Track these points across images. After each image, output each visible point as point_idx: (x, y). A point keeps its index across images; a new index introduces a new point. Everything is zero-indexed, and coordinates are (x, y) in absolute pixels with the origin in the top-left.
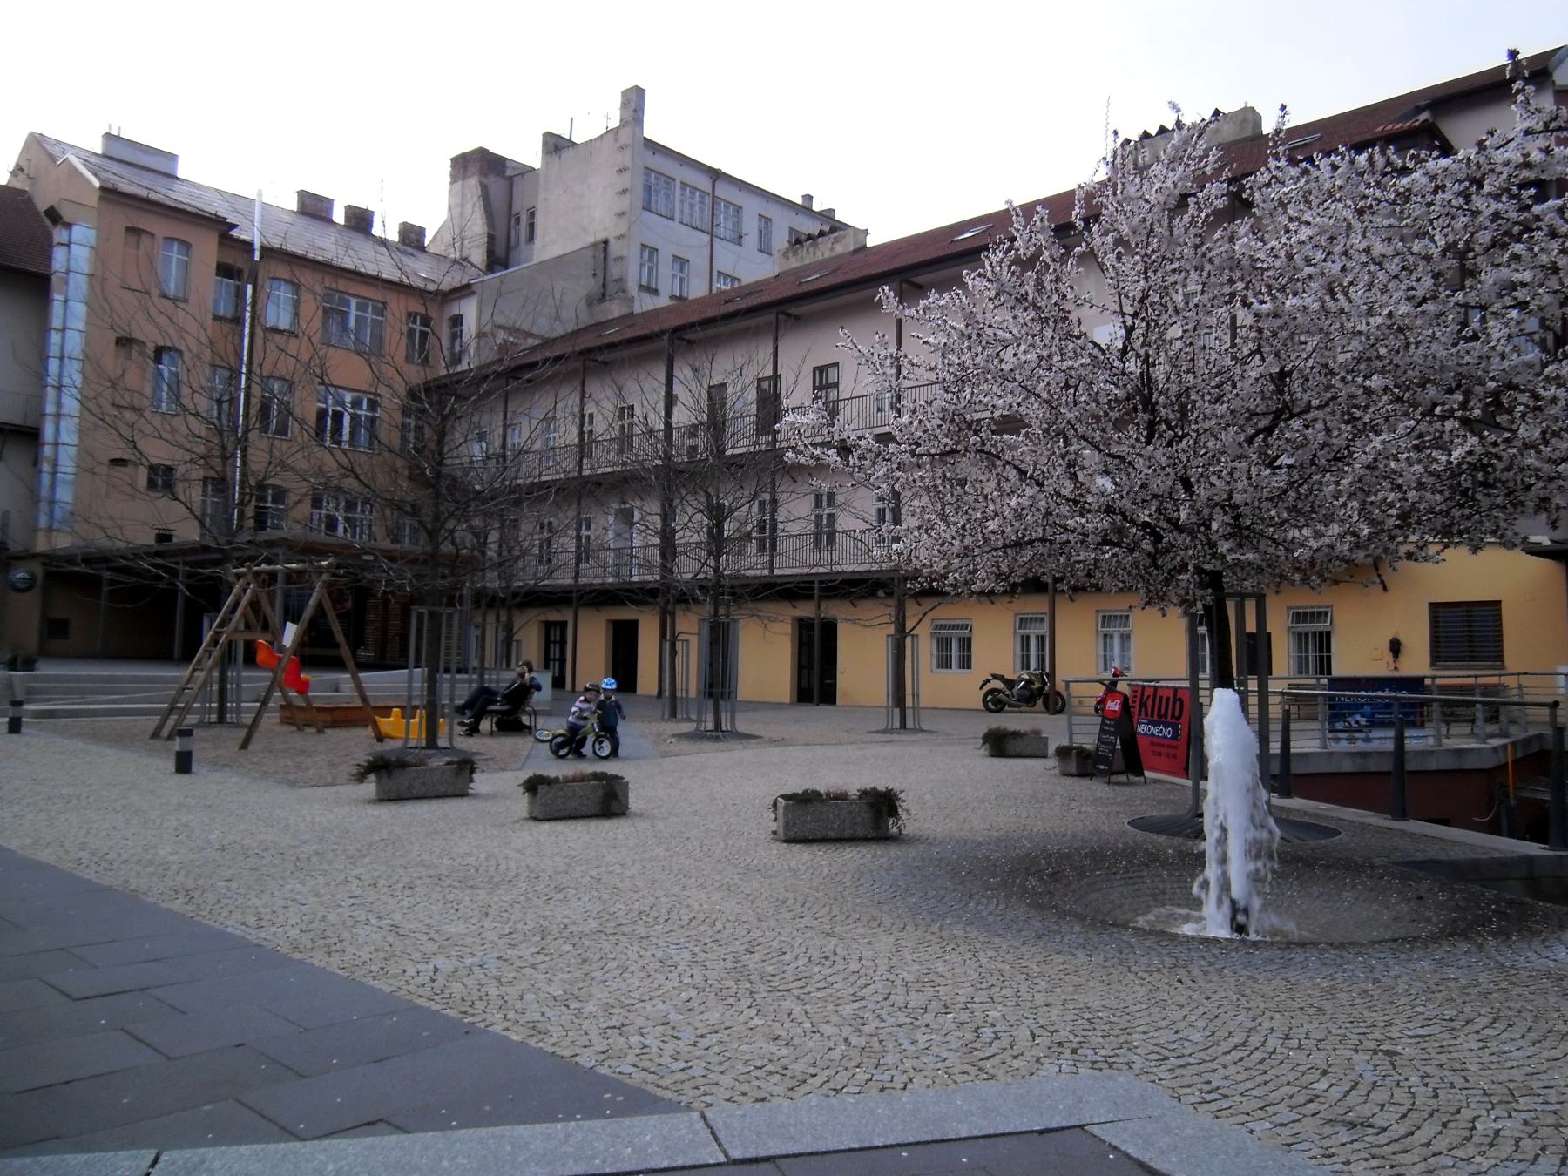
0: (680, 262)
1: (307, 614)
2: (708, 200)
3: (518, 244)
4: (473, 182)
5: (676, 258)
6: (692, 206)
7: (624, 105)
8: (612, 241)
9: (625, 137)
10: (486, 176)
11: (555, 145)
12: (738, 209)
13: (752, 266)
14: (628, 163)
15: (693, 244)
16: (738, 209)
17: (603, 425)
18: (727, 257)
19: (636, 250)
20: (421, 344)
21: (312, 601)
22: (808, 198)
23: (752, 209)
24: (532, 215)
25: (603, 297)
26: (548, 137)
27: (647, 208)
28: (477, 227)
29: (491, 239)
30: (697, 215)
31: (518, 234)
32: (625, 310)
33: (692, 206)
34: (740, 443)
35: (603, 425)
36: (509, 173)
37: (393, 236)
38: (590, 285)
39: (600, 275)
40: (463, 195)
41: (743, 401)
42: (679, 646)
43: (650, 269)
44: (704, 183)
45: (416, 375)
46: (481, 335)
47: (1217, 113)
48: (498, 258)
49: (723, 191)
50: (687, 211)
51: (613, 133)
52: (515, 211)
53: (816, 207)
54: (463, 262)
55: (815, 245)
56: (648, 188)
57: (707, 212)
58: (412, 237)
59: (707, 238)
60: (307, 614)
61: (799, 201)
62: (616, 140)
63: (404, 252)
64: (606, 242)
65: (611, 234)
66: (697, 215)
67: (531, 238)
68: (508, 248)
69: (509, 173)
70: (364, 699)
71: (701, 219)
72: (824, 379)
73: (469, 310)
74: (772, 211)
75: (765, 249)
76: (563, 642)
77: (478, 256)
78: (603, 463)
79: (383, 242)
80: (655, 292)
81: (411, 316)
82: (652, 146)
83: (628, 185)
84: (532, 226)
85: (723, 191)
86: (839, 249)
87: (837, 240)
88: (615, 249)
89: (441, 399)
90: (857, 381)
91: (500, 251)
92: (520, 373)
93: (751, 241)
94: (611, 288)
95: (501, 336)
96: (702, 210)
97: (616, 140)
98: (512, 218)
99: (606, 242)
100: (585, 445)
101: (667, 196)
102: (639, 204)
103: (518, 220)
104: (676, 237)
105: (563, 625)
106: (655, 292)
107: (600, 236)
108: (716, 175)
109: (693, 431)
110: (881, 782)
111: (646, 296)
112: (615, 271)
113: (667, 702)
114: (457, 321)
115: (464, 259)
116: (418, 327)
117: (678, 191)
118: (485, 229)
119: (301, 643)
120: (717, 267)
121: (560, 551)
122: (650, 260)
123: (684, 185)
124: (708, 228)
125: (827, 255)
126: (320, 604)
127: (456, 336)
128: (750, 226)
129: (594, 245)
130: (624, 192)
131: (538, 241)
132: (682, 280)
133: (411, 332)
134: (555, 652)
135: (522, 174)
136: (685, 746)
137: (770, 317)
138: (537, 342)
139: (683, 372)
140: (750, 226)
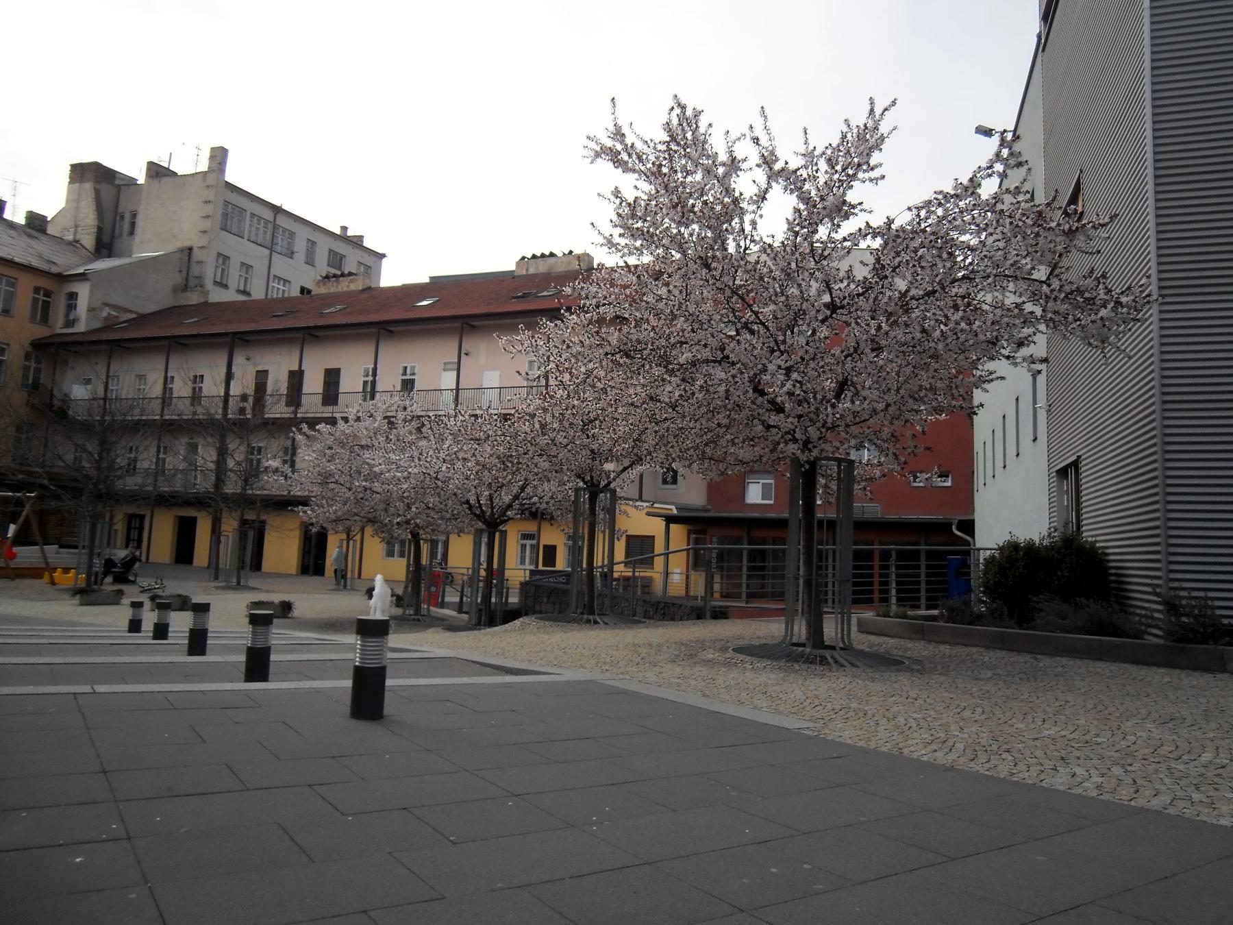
0: (247, 267)
1: (22, 519)
2: (270, 226)
3: (121, 235)
4: (88, 187)
5: (243, 264)
6: (258, 229)
7: (212, 158)
8: (196, 250)
9: (211, 180)
10: (99, 183)
11: (157, 171)
12: (292, 234)
13: (299, 275)
14: (211, 198)
15: (257, 256)
16: (292, 234)
17: (181, 389)
18: (281, 266)
19: (213, 257)
20: (43, 312)
21: (24, 513)
22: (344, 229)
23: (302, 235)
24: (134, 216)
25: (185, 288)
26: (151, 165)
27: (224, 228)
28: (89, 219)
29: (100, 230)
30: (261, 236)
31: (121, 227)
32: (202, 300)
33: (258, 229)
34: (277, 410)
35: (181, 389)
36: (117, 182)
37: (21, 219)
38: (178, 279)
39: (185, 272)
40: (79, 194)
41: (278, 380)
42: (222, 538)
43: (223, 270)
44: (268, 215)
45: (40, 332)
46: (91, 310)
47: (571, 252)
48: (105, 246)
49: (281, 221)
50: (253, 233)
51: (204, 174)
52: (120, 210)
53: (349, 234)
54: (74, 244)
55: (338, 282)
56: (225, 216)
57: (269, 233)
58: (36, 223)
59: (267, 252)
60: (22, 519)
61: (338, 232)
62: (204, 180)
63: (30, 236)
64: (191, 249)
65: (195, 241)
66: (261, 236)
67: (132, 232)
68: (113, 237)
69: (117, 182)
70: (47, 563)
71: (264, 238)
72: (332, 378)
73: (83, 292)
74: (316, 237)
75: (310, 262)
76: (141, 529)
77: (89, 241)
78: (182, 408)
79: (12, 225)
80: (226, 287)
81: (37, 290)
82: (228, 185)
83: (210, 213)
84: (133, 225)
85: (281, 221)
86: (353, 287)
87: (351, 281)
88: (197, 255)
89: (55, 351)
90: (351, 382)
91: (106, 239)
92: (117, 342)
93: (301, 255)
94: (192, 282)
95: (106, 312)
96: (265, 233)
97: (204, 180)
98: (118, 215)
99: (191, 249)
100: (167, 398)
101: (240, 221)
102: (218, 226)
103: (122, 217)
104: (243, 250)
105: (142, 517)
106: (226, 287)
107: (187, 244)
108: (277, 210)
109: (244, 398)
110: (286, 598)
111: (219, 290)
112: (196, 270)
113: (213, 571)
114: (73, 296)
115: (77, 242)
116: (41, 297)
117: (248, 218)
118: (96, 222)
119: (18, 534)
120: (273, 272)
121: (143, 462)
122: (224, 263)
123: (253, 215)
124: (269, 244)
125: (345, 289)
126: (27, 517)
127: (71, 307)
128: (300, 246)
129: (182, 250)
130: (207, 217)
131: (138, 238)
132: (246, 279)
133: (35, 301)
134: (134, 534)
135: (128, 185)
136: (219, 591)
137: (300, 335)
138: (134, 316)
139: (239, 360)
140: (300, 246)
